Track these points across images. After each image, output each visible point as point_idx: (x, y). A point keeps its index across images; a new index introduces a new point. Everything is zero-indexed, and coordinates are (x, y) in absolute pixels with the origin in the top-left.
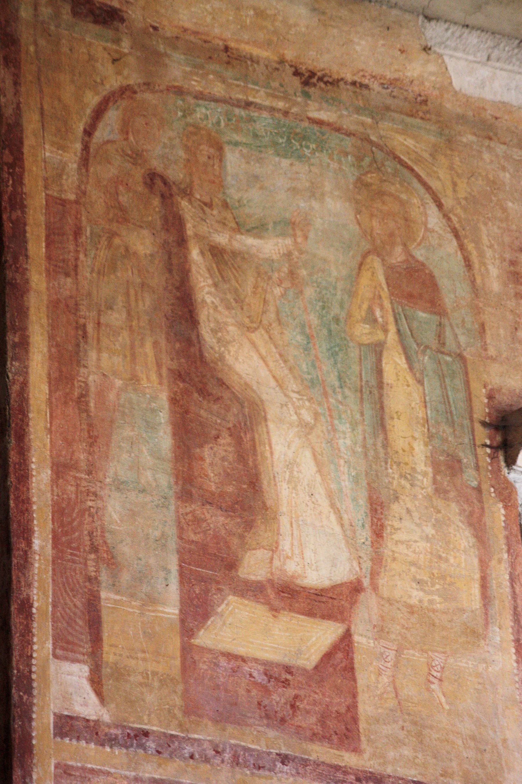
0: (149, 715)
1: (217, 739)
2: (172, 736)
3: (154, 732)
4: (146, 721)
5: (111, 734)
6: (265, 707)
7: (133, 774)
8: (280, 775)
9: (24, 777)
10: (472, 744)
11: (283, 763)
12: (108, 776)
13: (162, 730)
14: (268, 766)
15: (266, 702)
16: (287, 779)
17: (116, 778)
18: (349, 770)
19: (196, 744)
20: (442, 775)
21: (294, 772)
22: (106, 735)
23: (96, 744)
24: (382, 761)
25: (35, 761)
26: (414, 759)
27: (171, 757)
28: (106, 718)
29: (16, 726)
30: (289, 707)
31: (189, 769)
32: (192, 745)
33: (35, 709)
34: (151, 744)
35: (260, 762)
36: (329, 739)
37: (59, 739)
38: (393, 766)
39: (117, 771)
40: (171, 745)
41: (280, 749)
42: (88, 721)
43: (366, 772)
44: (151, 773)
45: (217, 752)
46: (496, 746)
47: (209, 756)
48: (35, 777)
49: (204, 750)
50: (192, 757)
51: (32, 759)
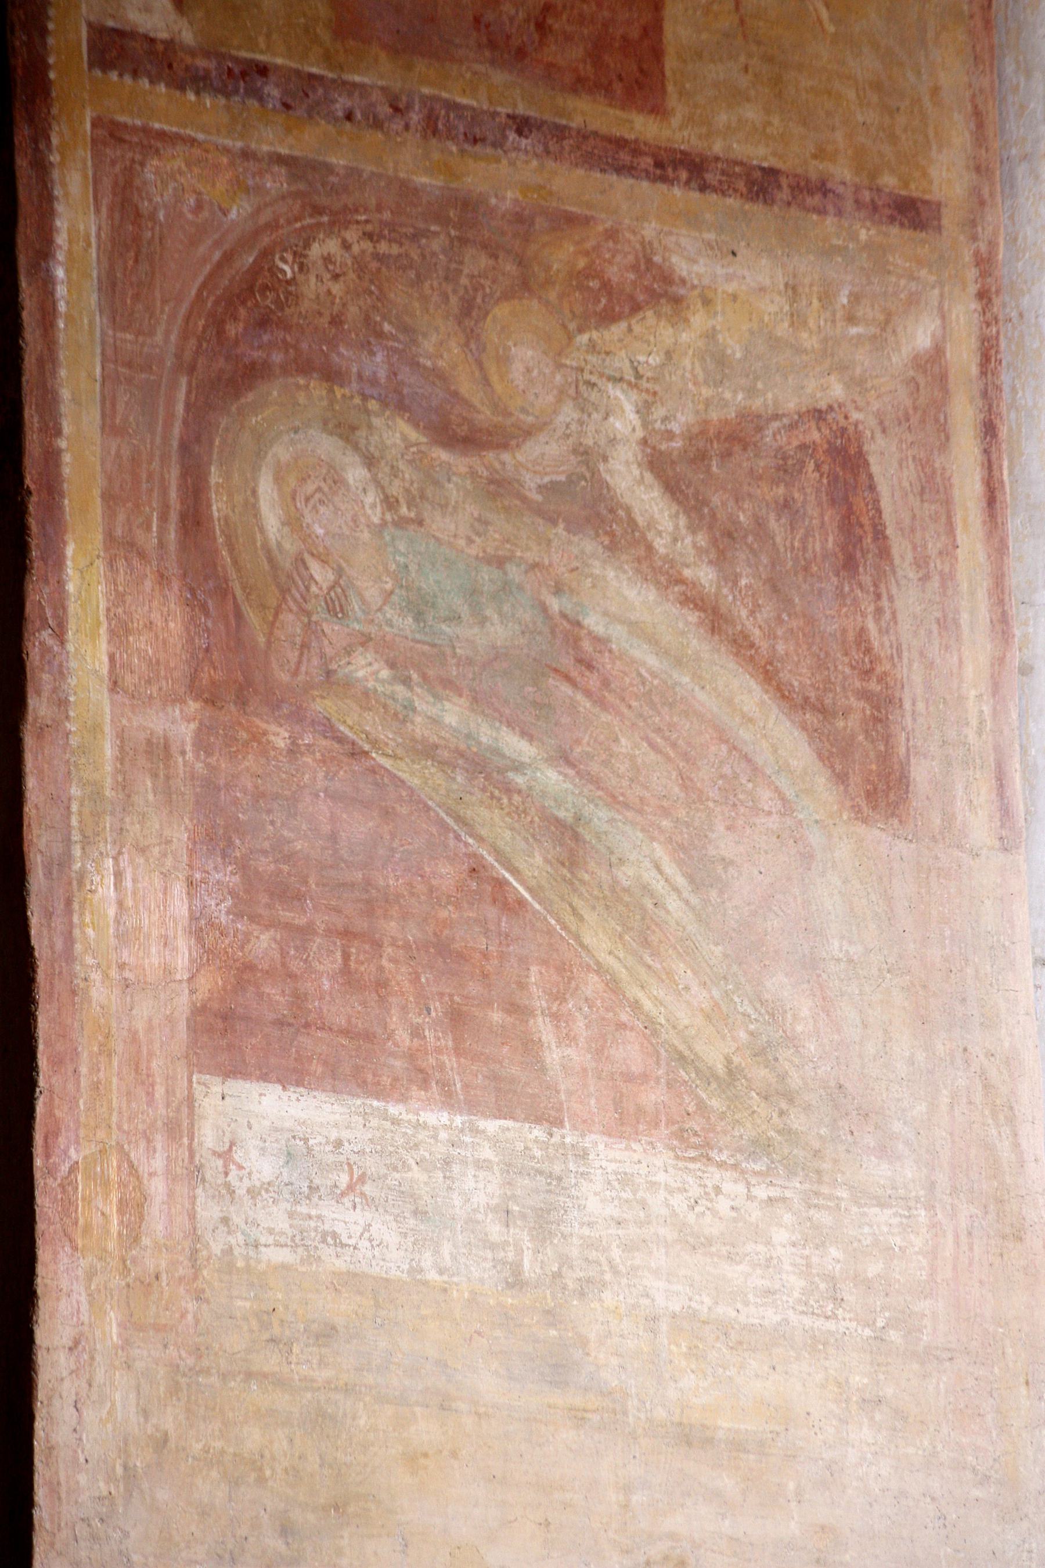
0: (268, 36)
1: (397, 85)
2: (311, 76)
3: (277, 67)
4: (263, 45)
5: (197, 68)
6: (488, 26)
7: (239, 144)
8: (514, 155)
9: (35, 141)
10: (875, 98)
11: (520, 132)
12: (192, 145)
13: (294, 65)
14: (491, 138)
15: (490, 16)
16: (527, 162)
17: (207, 151)
18: (642, 146)
19: (357, 94)
20: (815, 157)
21: (540, 149)
22: (187, 69)
23: (167, 85)
24: (704, 130)
25: (55, 111)
26: (764, 128)
27: (310, 117)
28: (188, 37)
29: (18, 43)
30: (532, 27)
31: (344, 140)
32: (350, 95)
33: (52, 12)
34: (273, 91)
35: (477, 130)
36: (606, 90)
37: (98, 73)
38: (725, 139)
39: (209, 138)
40: (310, 94)
41: (515, 105)
42: (152, 41)
43: (674, 151)
44: (271, 144)
45: (396, 109)
46: (919, 100)
47: (382, 116)
48: (55, 141)
49: (373, 105)
50: (349, 117)
51: (49, 108)
